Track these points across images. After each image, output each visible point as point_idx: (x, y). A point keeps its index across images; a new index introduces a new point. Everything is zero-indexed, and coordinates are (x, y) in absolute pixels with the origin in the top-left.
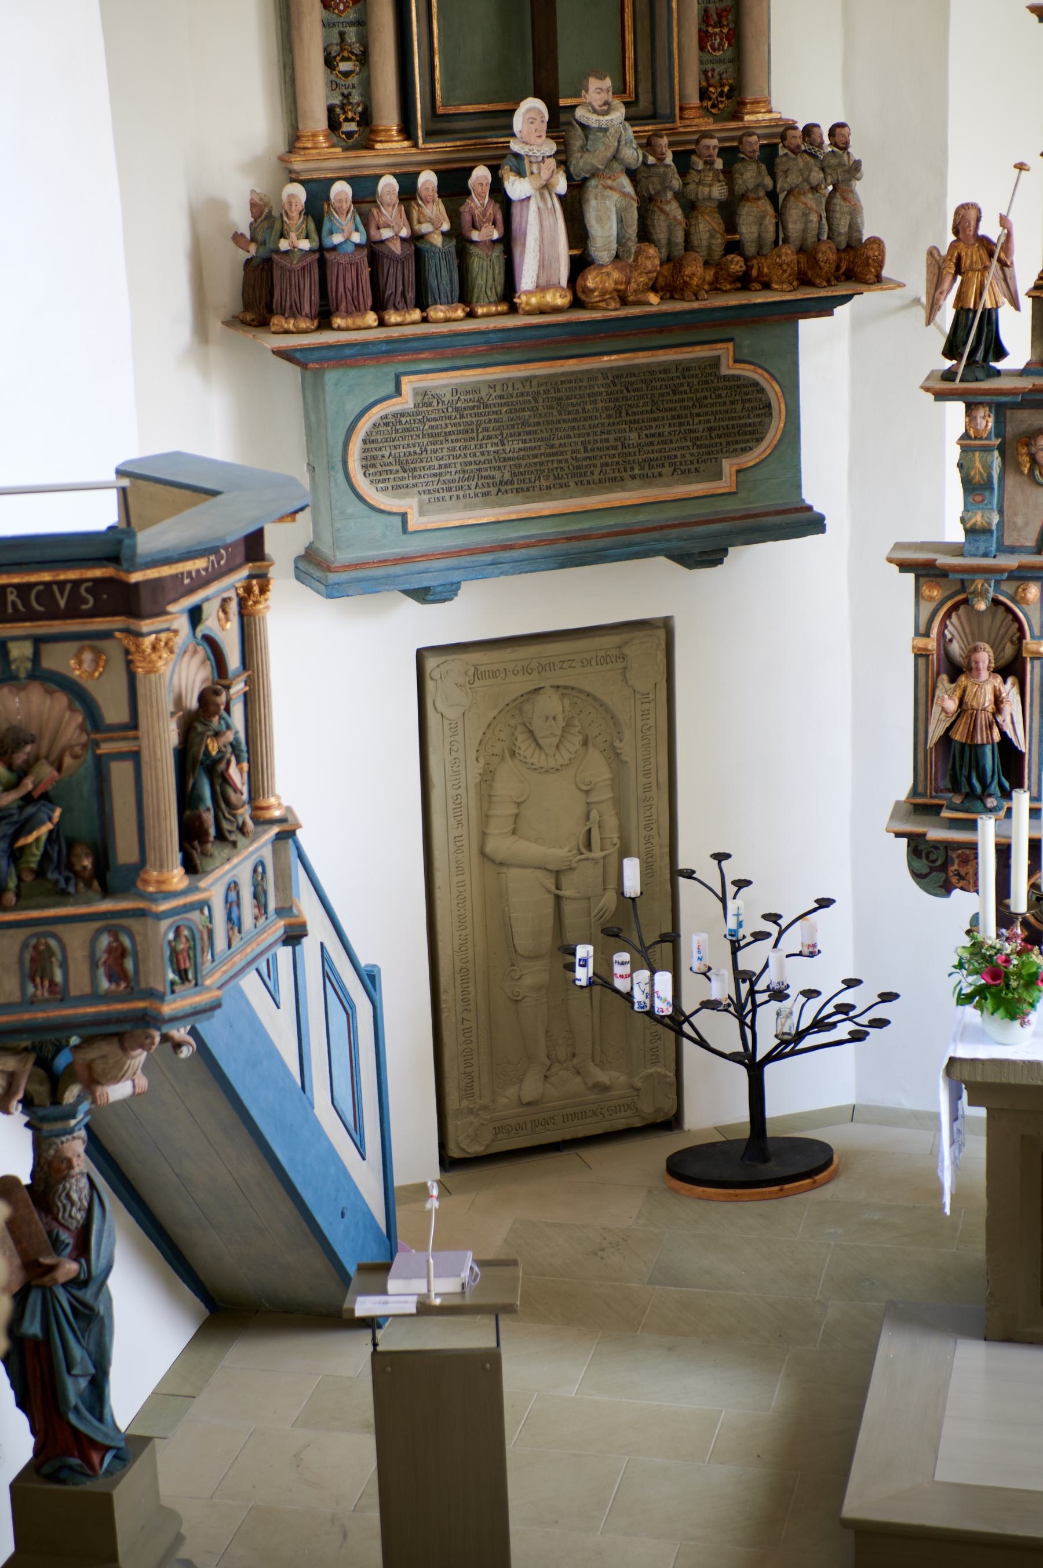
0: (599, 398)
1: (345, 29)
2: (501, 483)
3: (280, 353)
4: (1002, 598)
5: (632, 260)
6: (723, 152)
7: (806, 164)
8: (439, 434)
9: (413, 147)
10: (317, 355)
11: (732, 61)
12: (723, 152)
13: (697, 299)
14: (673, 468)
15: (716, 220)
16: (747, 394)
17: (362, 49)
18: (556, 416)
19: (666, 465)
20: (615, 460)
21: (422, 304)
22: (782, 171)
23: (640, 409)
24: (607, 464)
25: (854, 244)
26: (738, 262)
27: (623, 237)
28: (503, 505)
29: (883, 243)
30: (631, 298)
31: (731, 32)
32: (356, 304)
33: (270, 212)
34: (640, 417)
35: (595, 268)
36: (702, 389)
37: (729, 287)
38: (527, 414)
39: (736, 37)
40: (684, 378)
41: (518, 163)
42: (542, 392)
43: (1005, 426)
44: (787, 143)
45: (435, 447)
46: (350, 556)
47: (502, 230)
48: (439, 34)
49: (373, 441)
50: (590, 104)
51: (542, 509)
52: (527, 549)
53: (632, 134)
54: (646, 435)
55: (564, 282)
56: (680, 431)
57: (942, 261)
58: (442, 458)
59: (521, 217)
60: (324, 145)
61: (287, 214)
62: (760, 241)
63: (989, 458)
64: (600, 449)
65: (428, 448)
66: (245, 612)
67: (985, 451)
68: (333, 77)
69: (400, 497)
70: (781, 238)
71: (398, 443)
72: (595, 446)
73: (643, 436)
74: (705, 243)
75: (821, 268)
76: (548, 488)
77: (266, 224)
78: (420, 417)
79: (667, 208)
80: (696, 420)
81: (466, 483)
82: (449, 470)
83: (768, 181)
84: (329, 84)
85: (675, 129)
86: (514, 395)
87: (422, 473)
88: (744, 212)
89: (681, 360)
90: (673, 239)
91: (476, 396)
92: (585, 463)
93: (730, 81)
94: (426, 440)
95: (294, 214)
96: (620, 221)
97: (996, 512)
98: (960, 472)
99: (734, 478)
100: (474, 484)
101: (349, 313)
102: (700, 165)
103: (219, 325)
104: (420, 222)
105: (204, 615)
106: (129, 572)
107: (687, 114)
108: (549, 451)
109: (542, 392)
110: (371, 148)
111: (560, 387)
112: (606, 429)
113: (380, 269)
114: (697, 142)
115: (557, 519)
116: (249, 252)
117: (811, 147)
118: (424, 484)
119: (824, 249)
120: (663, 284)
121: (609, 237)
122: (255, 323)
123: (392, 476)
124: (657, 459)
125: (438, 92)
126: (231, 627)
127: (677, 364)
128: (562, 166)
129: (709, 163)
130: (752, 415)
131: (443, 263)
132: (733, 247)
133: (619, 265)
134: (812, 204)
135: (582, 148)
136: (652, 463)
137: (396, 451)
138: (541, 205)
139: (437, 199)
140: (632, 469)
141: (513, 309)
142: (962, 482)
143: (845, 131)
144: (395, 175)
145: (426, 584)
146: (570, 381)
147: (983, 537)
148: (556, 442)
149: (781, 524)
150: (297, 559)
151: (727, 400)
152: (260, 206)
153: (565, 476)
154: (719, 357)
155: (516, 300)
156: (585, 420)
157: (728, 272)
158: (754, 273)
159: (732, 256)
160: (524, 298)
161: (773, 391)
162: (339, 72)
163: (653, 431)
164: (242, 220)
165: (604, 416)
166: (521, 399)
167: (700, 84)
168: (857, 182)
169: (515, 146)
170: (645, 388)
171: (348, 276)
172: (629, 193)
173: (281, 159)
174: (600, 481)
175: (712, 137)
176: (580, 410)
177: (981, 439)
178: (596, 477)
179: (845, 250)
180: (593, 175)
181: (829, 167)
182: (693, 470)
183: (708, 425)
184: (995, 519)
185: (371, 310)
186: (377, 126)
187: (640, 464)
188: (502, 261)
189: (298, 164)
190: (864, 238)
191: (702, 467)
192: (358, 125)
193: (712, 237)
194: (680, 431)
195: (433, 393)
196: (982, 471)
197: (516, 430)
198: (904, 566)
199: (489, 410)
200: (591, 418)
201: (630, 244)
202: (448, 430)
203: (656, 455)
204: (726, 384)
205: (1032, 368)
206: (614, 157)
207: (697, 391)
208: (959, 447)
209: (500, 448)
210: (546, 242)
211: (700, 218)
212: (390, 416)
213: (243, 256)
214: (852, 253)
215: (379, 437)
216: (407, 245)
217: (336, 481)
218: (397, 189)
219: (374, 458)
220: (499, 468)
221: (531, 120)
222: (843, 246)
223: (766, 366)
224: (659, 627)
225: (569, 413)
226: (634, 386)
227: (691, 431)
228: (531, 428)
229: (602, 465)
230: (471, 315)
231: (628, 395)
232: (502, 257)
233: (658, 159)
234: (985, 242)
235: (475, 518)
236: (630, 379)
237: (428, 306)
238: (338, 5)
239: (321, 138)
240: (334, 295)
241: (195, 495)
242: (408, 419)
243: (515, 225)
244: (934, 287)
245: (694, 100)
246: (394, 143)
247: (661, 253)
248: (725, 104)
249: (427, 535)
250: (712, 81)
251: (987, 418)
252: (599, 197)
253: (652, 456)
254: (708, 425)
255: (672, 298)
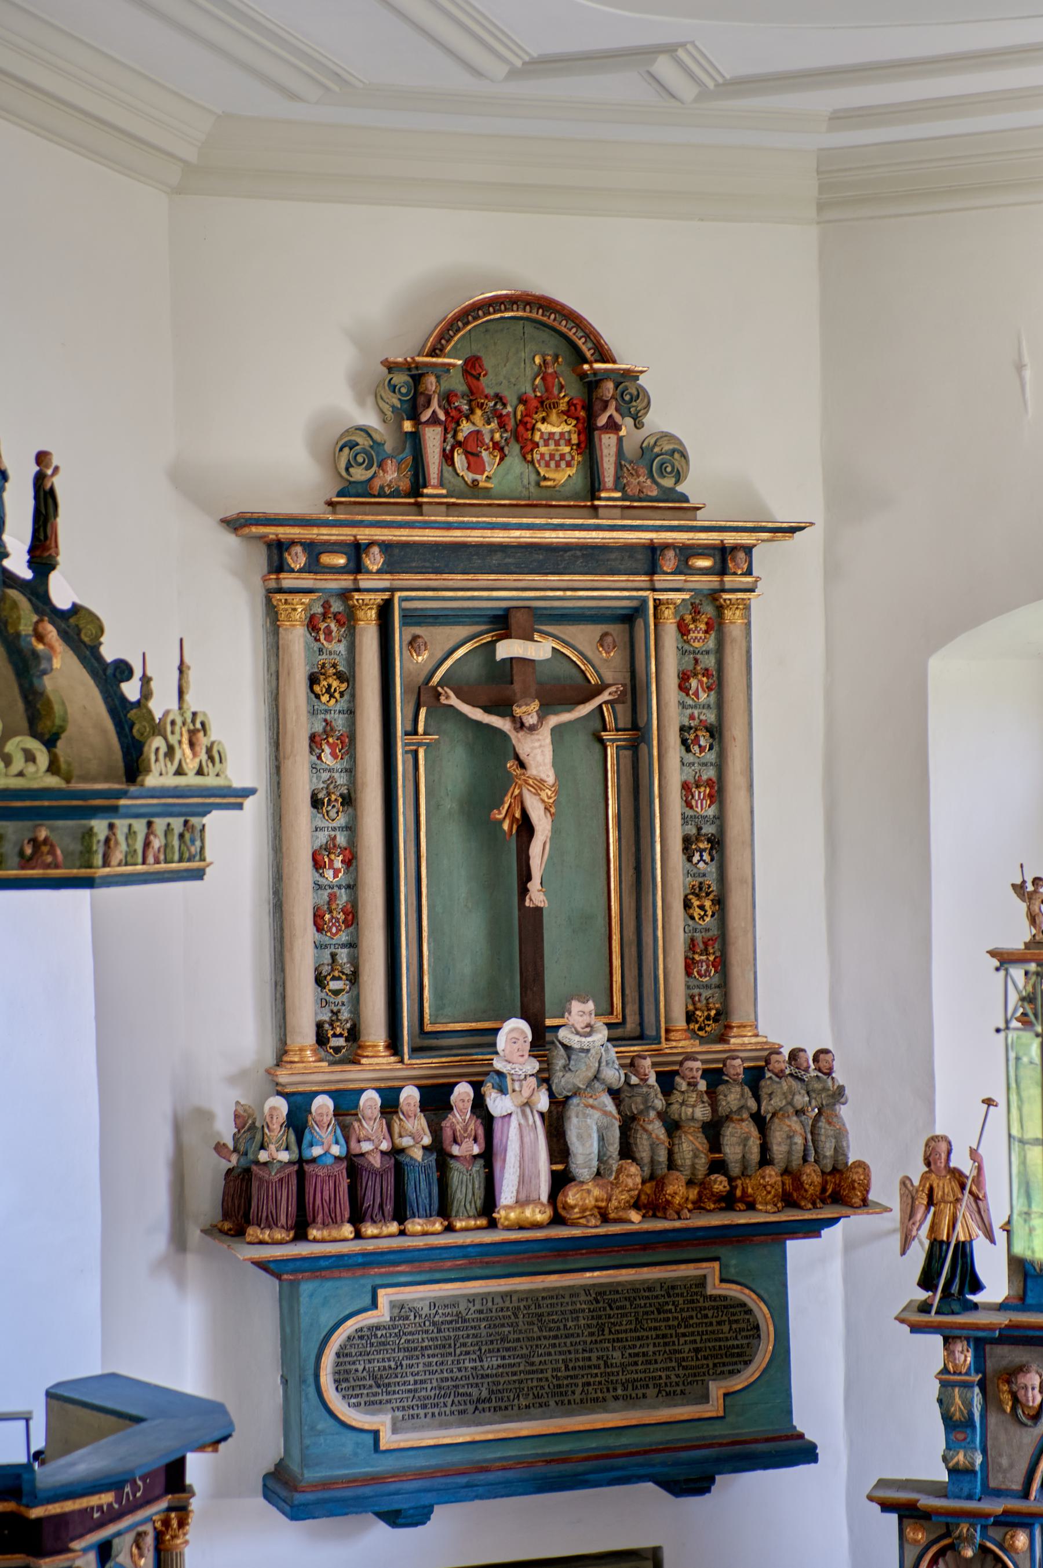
0: (581, 1315)
1: (336, 951)
2: (478, 1400)
3: (262, 1265)
4: (989, 1544)
5: (613, 1177)
6: (706, 1073)
7: (790, 1087)
8: (416, 1349)
9: (399, 1062)
10: (291, 1266)
11: (718, 987)
12: (706, 1073)
13: (680, 1218)
14: (657, 1390)
15: (699, 1140)
16: (733, 1314)
17: (352, 969)
18: (537, 1333)
19: (651, 1386)
20: (597, 1379)
21: (400, 1216)
22: (766, 1094)
23: (623, 1328)
24: (589, 1384)
25: (840, 1167)
26: (721, 1182)
27: (605, 1155)
28: (479, 1424)
29: (868, 1167)
30: (612, 1216)
31: (717, 960)
32: (333, 1216)
33: (254, 1123)
34: (624, 1335)
35: (576, 1185)
36: (688, 1308)
37: (712, 1206)
38: (506, 1329)
39: (722, 964)
40: (669, 1296)
41: (501, 1081)
42: (522, 1307)
43: (985, 1362)
44: (771, 1067)
45: (411, 1362)
46: (319, 1475)
47: (483, 1145)
48: (429, 956)
49: (347, 1355)
50: (573, 1025)
51: (521, 1429)
52: (504, 1471)
53: (615, 1055)
54: (630, 1354)
55: (544, 1198)
56: (665, 1351)
57: (914, 1191)
58: (417, 1374)
59: (502, 1133)
60: (311, 1059)
61: (268, 1127)
62: (744, 1160)
63: (969, 1395)
64: (581, 1368)
65: (404, 1363)
66: (162, 1547)
67: (965, 1387)
68: (323, 995)
69: (373, 1413)
70: (766, 1159)
71: (373, 1357)
72: (577, 1364)
73: (627, 1355)
74: (688, 1162)
75: (806, 1191)
76: (527, 1407)
77: (248, 1135)
78: (397, 1331)
79: (650, 1127)
80: (682, 1340)
81: (442, 1400)
82: (424, 1386)
83: (752, 1104)
84: (319, 1002)
85: (661, 1050)
86: (494, 1310)
87: (397, 1389)
88: (728, 1133)
89: (666, 1279)
90: (656, 1158)
91: (455, 1311)
92: (565, 1382)
93: (717, 1006)
94: (401, 1355)
95: (275, 1127)
96: (602, 1139)
97: (979, 1452)
98: (940, 1408)
99: (721, 1401)
100: (450, 1401)
101: (325, 1225)
102: (684, 1087)
103: (198, 1232)
104: (401, 1136)
105: (114, 1552)
106: (29, 1507)
107: (673, 1035)
108: (529, 1368)
109: (522, 1307)
110: (356, 1062)
111: (541, 1302)
112: (588, 1347)
113: (359, 1181)
114: (681, 1063)
115: (536, 1440)
116: (230, 1161)
117: (797, 1070)
118: (398, 1401)
119: (808, 1171)
120: (646, 1202)
121: (590, 1154)
122: (232, 1232)
123: (365, 1392)
124: (641, 1379)
125: (427, 1010)
126: (145, 1564)
127: (662, 1283)
128: (545, 1085)
129: (692, 1085)
130: (739, 1337)
131: (422, 1177)
132: (718, 1166)
133: (601, 1182)
134: (797, 1127)
135: (564, 1067)
136: (635, 1384)
137: (371, 1365)
138: (522, 1122)
139: (419, 1114)
140: (615, 1389)
141: (493, 1224)
142: (943, 1418)
143: (829, 1057)
144: (378, 1090)
145: (396, 1507)
146: (552, 1297)
147: (968, 1478)
148: (537, 1360)
149: (770, 1452)
150: (266, 1477)
151: (714, 1320)
152: (244, 1117)
153: (545, 1395)
154: (705, 1276)
155: (495, 1215)
156: (566, 1337)
157: (712, 1192)
158: (739, 1193)
159: (716, 1175)
160: (503, 1213)
161: (761, 1311)
162: (329, 990)
163: (636, 1351)
164: (225, 1129)
165: (586, 1333)
166: (501, 1314)
167: (687, 1007)
168: (842, 1107)
169: (498, 1064)
170: (628, 1306)
171: (326, 1188)
172: (610, 1112)
173: (268, 1072)
174: (582, 1401)
175: (695, 1060)
176: (562, 1327)
177: (960, 1374)
178: (577, 1397)
179: (831, 1173)
180: (575, 1094)
181: (814, 1091)
182: (679, 1392)
183: (694, 1346)
184: (979, 1459)
185: (348, 1222)
186: (365, 1042)
187: (623, 1384)
188: (483, 1176)
189: (284, 1076)
190: (850, 1162)
191: (688, 1389)
192: (347, 1040)
193: (695, 1156)
194: (665, 1351)
195: (410, 1306)
196: (962, 1408)
197: (495, 1346)
198: (886, 1507)
199: (468, 1324)
200: (572, 1335)
201: (611, 1162)
202: (424, 1344)
203: (640, 1376)
204: (713, 1304)
205: (1010, 1301)
206: (595, 1077)
207: (682, 1310)
208: (938, 1381)
209: (478, 1364)
210: (526, 1158)
211: (683, 1137)
212: (365, 1329)
213: (225, 1165)
214: (838, 1176)
215: (353, 1351)
216: (387, 1158)
217: (307, 1395)
218: (379, 1105)
219: (347, 1372)
220: (477, 1385)
221: (514, 1040)
222: (829, 1169)
223: (754, 1287)
224: (647, 1559)
225: (550, 1330)
226: (618, 1304)
227: (676, 1351)
228: (510, 1345)
229: (584, 1385)
230: (450, 1229)
231: (612, 1313)
232: (482, 1171)
233: (641, 1080)
234: (957, 1175)
235: (451, 1437)
236: (612, 1297)
237: (406, 1219)
238: (331, 928)
239: (308, 1052)
240: (311, 1206)
241: (121, 1421)
242: (384, 1332)
243: (496, 1140)
244: (907, 1217)
245: (680, 1022)
246: (380, 1059)
247: (643, 1171)
248: (712, 1027)
249: (399, 1454)
250: (699, 1005)
251: (966, 1352)
252: (580, 1115)
253: (636, 1376)
254: (694, 1346)
255: (654, 1216)
